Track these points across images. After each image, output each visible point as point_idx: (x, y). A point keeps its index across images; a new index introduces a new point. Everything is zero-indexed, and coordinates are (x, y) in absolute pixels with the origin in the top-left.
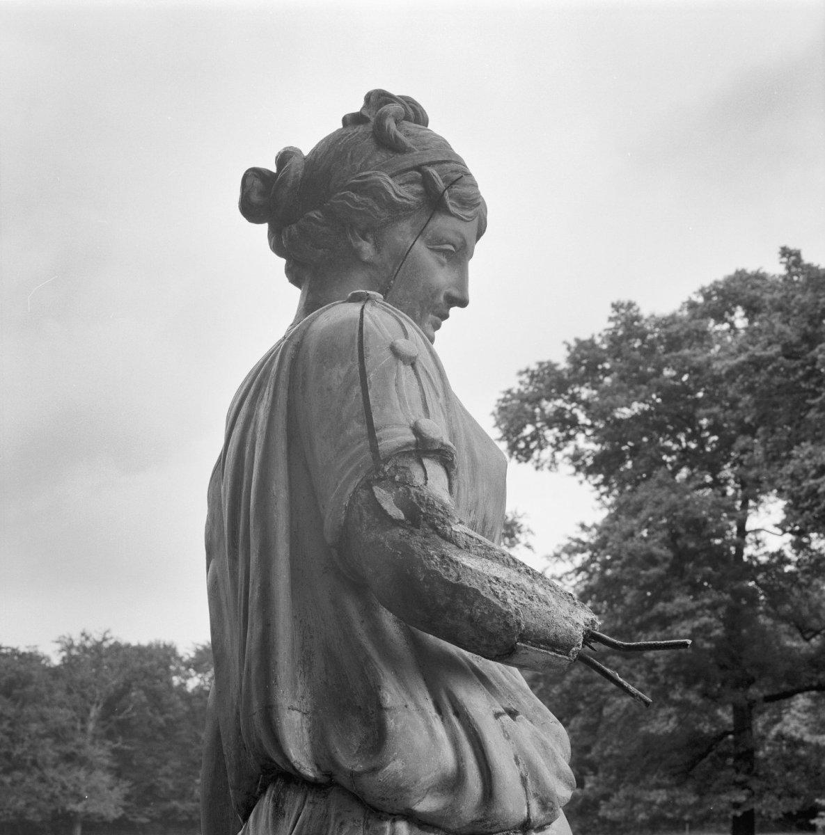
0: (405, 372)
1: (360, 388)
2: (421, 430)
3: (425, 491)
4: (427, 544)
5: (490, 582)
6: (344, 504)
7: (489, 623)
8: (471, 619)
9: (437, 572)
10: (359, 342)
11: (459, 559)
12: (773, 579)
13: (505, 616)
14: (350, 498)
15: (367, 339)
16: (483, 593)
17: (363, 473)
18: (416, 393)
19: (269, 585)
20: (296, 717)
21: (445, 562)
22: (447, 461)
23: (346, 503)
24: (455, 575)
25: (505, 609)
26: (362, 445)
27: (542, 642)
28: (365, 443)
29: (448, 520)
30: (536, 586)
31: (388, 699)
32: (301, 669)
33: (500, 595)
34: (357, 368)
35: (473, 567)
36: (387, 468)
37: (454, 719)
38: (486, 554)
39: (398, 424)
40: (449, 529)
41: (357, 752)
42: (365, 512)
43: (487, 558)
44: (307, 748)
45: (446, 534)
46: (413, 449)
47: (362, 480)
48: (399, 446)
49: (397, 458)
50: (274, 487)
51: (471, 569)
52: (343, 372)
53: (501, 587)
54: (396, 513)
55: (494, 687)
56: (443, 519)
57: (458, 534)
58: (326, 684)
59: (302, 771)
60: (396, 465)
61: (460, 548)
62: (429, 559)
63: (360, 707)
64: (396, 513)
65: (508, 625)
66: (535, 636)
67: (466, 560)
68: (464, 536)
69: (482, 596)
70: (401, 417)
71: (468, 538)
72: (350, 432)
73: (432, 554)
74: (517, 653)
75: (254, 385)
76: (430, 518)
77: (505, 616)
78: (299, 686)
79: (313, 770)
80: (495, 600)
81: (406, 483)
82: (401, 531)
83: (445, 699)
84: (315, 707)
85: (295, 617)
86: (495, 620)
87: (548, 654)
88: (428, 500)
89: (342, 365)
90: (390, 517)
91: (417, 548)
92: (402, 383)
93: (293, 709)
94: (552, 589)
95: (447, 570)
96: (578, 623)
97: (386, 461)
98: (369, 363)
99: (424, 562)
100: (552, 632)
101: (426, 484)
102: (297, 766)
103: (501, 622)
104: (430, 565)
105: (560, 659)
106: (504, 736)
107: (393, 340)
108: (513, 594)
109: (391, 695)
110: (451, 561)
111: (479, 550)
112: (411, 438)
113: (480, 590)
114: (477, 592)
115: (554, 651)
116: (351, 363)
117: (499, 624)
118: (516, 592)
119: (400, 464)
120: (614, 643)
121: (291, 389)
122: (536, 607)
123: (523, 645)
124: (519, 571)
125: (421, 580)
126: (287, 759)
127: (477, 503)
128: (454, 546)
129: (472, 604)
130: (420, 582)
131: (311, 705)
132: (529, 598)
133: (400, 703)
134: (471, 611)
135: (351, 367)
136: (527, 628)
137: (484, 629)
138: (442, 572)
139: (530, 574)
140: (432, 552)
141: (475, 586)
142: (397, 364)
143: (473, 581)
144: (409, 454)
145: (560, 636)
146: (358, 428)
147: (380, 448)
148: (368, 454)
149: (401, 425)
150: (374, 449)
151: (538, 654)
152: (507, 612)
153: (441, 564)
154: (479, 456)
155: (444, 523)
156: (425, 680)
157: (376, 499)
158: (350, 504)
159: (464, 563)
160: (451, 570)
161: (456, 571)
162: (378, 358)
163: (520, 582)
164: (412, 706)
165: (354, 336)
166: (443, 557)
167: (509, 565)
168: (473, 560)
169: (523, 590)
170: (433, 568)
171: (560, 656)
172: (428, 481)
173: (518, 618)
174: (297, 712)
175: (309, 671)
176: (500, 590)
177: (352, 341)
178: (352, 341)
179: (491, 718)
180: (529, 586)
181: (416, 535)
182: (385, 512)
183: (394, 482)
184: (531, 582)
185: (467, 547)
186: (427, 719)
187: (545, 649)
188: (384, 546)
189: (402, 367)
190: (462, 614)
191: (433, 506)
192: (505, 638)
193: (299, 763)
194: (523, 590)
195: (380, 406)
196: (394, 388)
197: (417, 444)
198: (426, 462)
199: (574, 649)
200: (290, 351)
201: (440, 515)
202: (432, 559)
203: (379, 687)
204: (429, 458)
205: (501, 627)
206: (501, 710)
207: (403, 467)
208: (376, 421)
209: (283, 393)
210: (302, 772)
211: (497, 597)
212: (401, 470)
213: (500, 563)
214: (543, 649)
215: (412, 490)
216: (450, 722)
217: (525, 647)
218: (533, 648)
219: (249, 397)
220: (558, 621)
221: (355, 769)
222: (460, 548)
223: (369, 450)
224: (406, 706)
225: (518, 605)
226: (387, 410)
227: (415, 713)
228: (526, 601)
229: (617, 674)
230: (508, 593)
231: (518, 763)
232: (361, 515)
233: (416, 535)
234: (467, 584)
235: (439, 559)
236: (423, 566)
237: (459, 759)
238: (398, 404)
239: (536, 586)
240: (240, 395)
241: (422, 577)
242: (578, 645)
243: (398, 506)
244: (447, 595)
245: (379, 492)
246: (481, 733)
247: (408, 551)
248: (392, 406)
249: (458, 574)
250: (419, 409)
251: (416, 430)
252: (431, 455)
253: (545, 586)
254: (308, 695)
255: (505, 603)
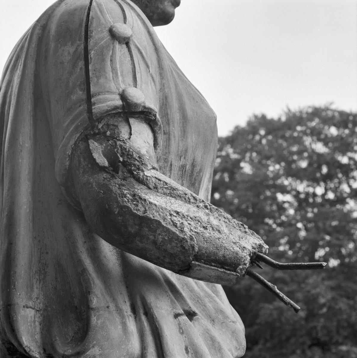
0: (120, 50)
1: (84, 62)
2: (127, 97)
3: (128, 144)
4: (123, 185)
5: (171, 215)
6: (68, 153)
7: (169, 246)
8: (155, 243)
9: (128, 207)
10: (86, 26)
11: (147, 197)
12: (145, 240)
13: (181, 241)
14: (72, 148)
15: (91, 23)
16: (163, 223)
17: (81, 130)
18: (129, 66)
19: (13, 213)
20: (30, 313)
21: (136, 199)
22: (151, 120)
23: (69, 152)
24: (143, 209)
25: (182, 236)
26: (81, 108)
27: (213, 261)
28: (84, 107)
29: (142, 167)
30: (212, 219)
31: (94, 302)
32: (37, 277)
33: (178, 225)
34: (82, 46)
35: (157, 204)
36: (100, 126)
37: (143, 318)
38: (170, 193)
39: (109, 92)
40: (142, 174)
41: (71, 340)
42: (82, 160)
43: (171, 196)
44: (38, 337)
45: (139, 178)
46: (120, 111)
47: (81, 135)
48: (108, 109)
49: (109, 118)
50: (20, 139)
51: (155, 205)
52: (72, 50)
53: (180, 219)
54: (102, 160)
55: (180, 294)
56: (138, 166)
57: (148, 178)
58: (55, 288)
59: (31, 353)
60: (107, 123)
61: (150, 188)
62: (122, 197)
63: (76, 307)
64: (102, 160)
65: (184, 248)
66: (207, 257)
67: (153, 198)
68: (154, 180)
69: (163, 226)
70: (112, 86)
71: (157, 181)
72: (74, 97)
73: (124, 192)
74: (193, 269)
75: (15, 56)
76: (129, 165)
77: (181, 241)
78: (35, 290)
79: (39, 353)
80: (173, 229)
81: (115, 137)
82: (105, 175)
83: (139, 303)
84: (46, 306)
85: (35, 238)
86: (174, 244)
87: (218, 270)
88: (129, 151)
89: (72, 44)
90: (97, 164)
91: (115, 189)
92: (116, 59)
93: (27, 307)
94: (226, 220)
95: (137, 206)
96: (244, 247)
97: (99, 120)
98: (91, 43)
99: (119, 199)
100: (221, 253)
101: (129, 138)
102: (27, 349)
103: (179, 245)
104: (123, 201)
105: (229, 275)
106: (179, 331)
107: (112, 24)
108: (189, 224)
109: (98, 298)
110: (140, 198)
111: (165, 190)
112: (119, 103)
113: (162, 221)
114: (159, 223)
115: (224, 268)
116: (78, 42)
117: (177, 247)
118: (192, 223)
119: (111, 122)
120: (273, 263)
121: (37, 62)
122: (208, 234)
123: (197, 263)
124: (198, 207)
125: (116, 213)
126: (21, 345)
127: (186, 151)
128: (145, 187)
129: (156, 232)
130: (115, 214)
131: (43, 304)
132: (204, 227)
133: (103, 304)
134: (155, 237)
135: (78, 46)
136: (200, 250)
137: (165, 251)
138: (132, 207)
139: (208, 209)
140: (125, 192)
141: (158, 218)
142: (113, 43)
143: (156, 214)
144: (119, 114)
145: (227, 257)
146: (80, 94)
147: (93, 111)
148: (85, 115)
149: (114, 93)
150: (89, 110)
151: (210, 270)
152: (183, 239)
153: (132, 201)
154: (189, 113)
155: (139, 169)
156: (127, 287)
157: (90, 149)
158: (72, 153)
159: (151, 201)
160: (140, 205)
161: (143, 206)
162: (100, 36)
163: (197, 215)
164: (112, 307)
165: (83, 20)
166: (134, 195)
167: (189, 202)
168: (159, 198)
169: (199, 221)
170: (125, 204)
171: (228, 272)
172: (132, 136)
173: (192, 243)
174: (31, 309)
175: (43, 279)
176: (179, 221)
177: (81, 25)
178: (81, 25)
179: (171, 318)
180: (204, 218)
181: (116, 178)
182: (94, 160)
183: (106, 136)
184: (208, 215)
185: (156, 188)
186: (123, 317)
187: (216, 267)
188: (92, 186)
189: (117, 45)
190: (148, 239)
191: (132, 156)
192: (182, 257)
193: (29, 348)
194: (199, 221)
195: (96, 77)
196: (109, 63)
197: (123, 107)
198: (132, 121)
199: (241, 267)
200: (37, 31)
201: (137, 163)
202: (125, 197)
203: (89, 292)
204: (134, 117)
205: (179, 250)
206: (181, 311)
207: (113, 125)
208: (93, 89)
209: (31, 65)
210: (31, 354)
211: (176, 226)
212: (112, 127)
213: (182, 200)
214: (214, 266)
215: (118, 143)
216: (140, 320)
217: (199, 265)
218: (205, 266)
219: (11, 66)
220: (226, 245)
221: (66, 353)
222: (150, 188)
223: (86, 112)
224: (108, 307)
225: (193, 233)
226: (102, 81)
227: (114, 312)
228: (200, 229)
229: (276, 287)
230: (186, 223)
231: (187, 352)
232: (79, 161)
233: (116, 178)
234: (151, 216)
235: (131, 197)
236: (118, 202)
237: (143, 347)
238: (111, 75)
239: (212, 219)
240: (9, 60)
241: (117, 211)
242: (245, 264)
243: (105, 156)
244: (135, 225)
245: (94, 145)
246: (161, 329)
247: (108, 190)
248: (106, 78)
249: (145, 208)
250: (130, 80)
251: (123, 97)
252: (137, 116)
253: (220, 218)
254: (41, 297)
255: (182, 231)
